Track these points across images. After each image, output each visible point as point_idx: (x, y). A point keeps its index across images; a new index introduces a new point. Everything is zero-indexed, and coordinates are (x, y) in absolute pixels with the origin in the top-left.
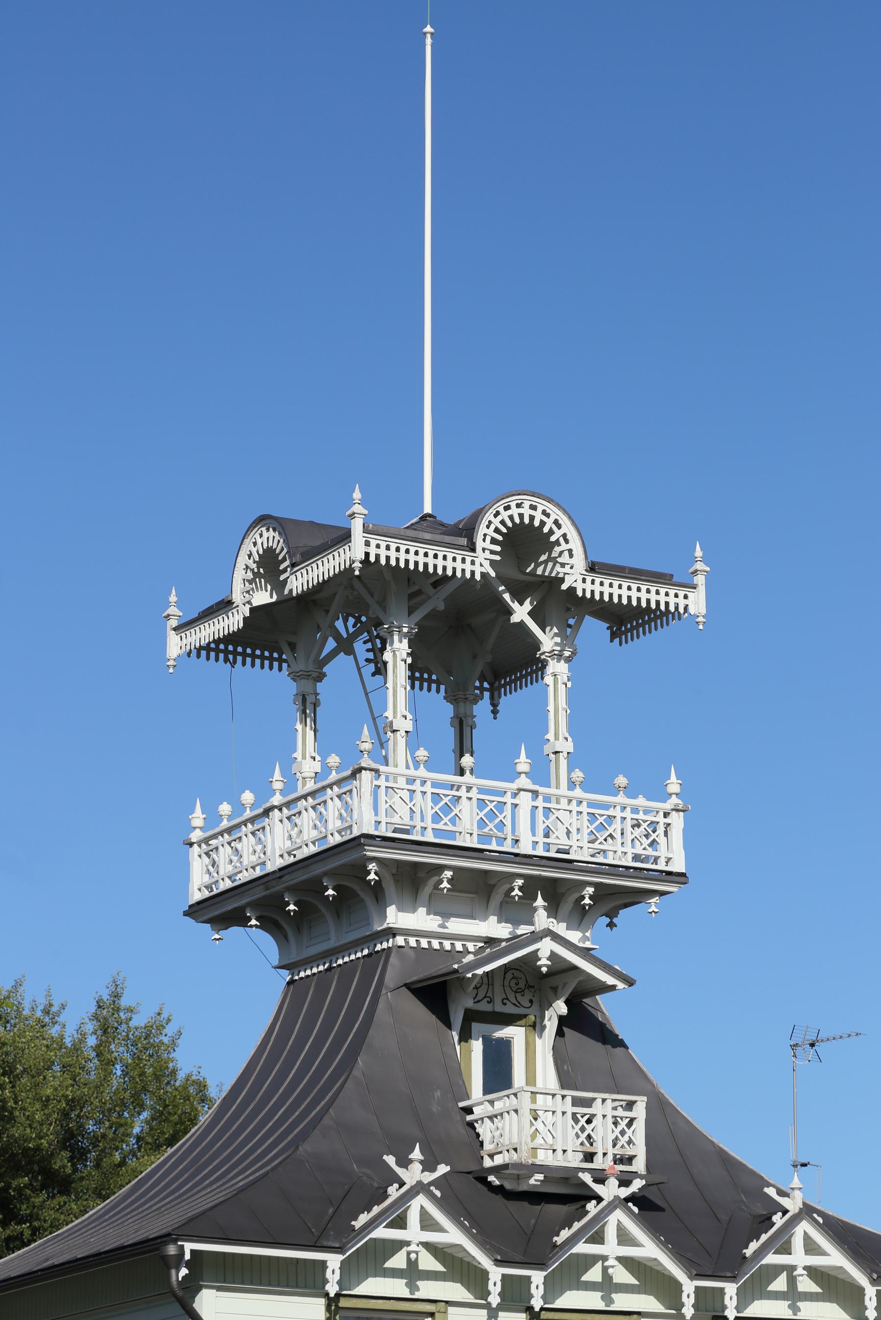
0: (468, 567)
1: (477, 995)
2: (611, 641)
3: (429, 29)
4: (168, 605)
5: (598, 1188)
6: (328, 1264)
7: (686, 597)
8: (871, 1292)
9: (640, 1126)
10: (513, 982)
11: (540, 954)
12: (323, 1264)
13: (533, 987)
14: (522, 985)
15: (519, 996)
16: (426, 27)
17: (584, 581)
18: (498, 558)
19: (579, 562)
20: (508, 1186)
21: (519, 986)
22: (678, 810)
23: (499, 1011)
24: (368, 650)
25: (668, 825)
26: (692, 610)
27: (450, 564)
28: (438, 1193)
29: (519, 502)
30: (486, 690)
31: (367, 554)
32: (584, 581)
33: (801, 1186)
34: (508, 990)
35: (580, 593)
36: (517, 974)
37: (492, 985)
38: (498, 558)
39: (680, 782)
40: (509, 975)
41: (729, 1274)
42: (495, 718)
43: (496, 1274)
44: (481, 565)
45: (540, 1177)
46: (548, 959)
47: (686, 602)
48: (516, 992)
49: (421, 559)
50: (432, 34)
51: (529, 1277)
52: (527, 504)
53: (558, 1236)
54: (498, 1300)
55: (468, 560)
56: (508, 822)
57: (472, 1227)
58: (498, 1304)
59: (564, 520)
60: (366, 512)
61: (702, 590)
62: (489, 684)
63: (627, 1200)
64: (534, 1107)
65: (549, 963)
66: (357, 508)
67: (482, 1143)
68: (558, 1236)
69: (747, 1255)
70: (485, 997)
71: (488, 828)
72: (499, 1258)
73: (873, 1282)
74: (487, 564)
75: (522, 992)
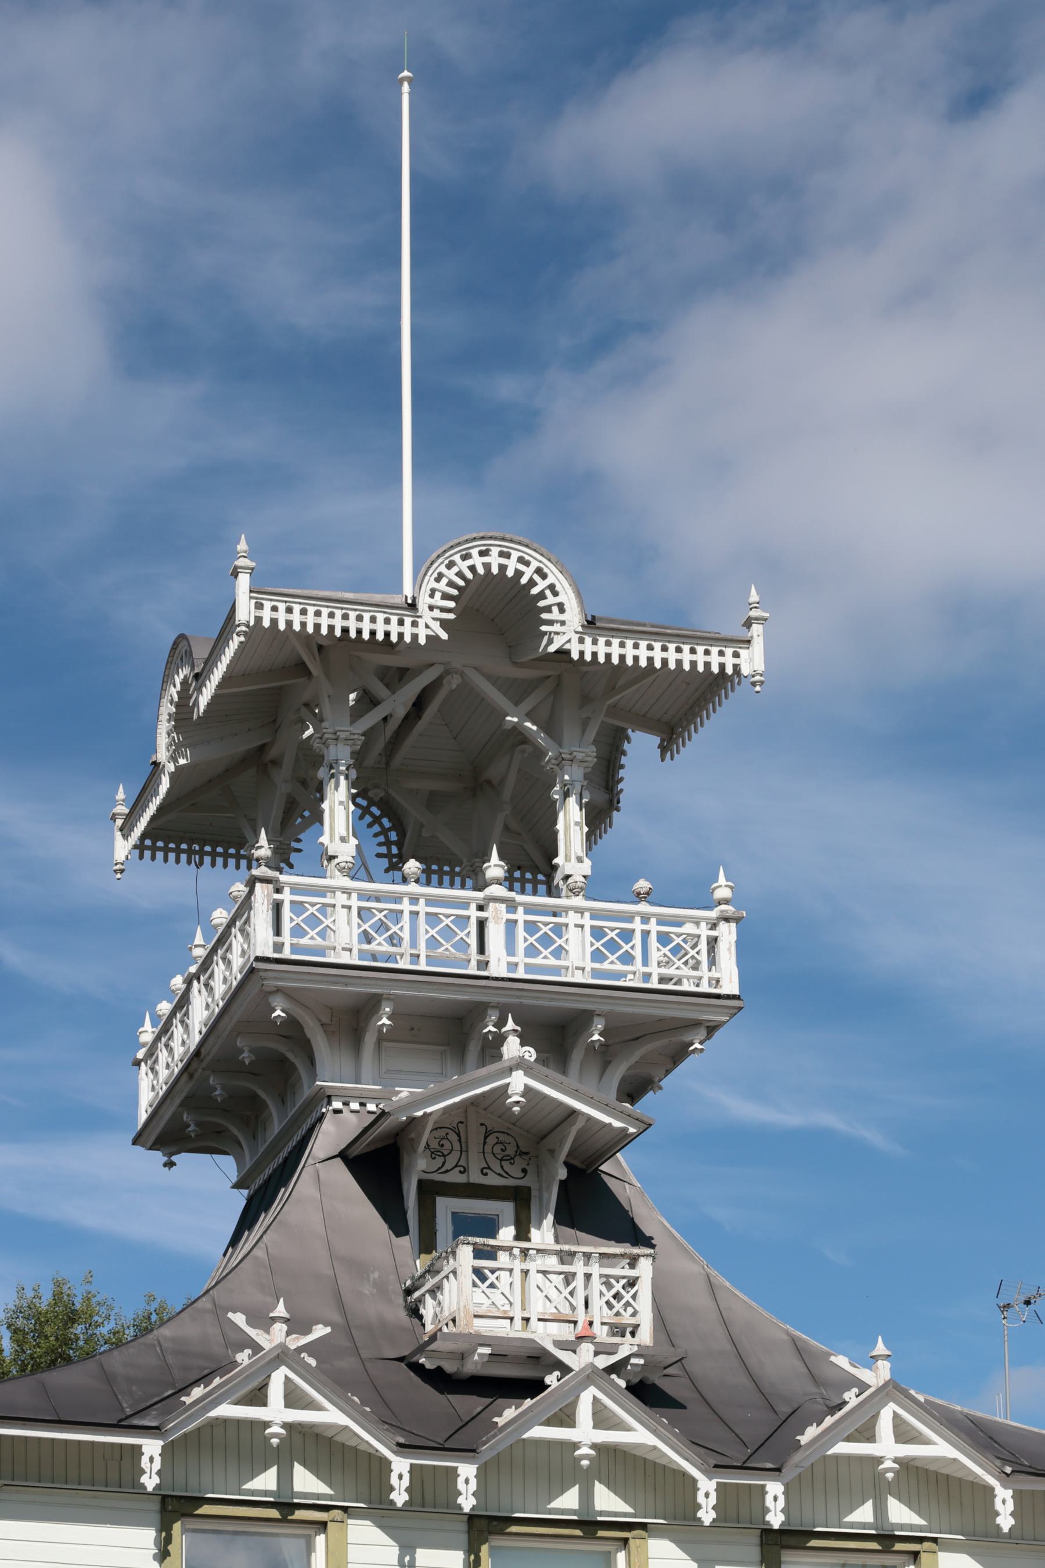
0: (408, 631)
1: (444, 1163)
2: (663, 760)
3: (406, 73)
4: (115, 803)
6: (144, 1450)
9: (645, 1288)
10: (497, 1149)
12: (137, 1451)
13: (527, 1154)
14: (511, 1150)
15: (506, 1164)
17: (581, 641)
19: (574, 617)
20: (450, 1367)
21: (506, 1153)
22: (727, 920)
23: (476, 1182)
24: (380, 844)
25: (716, 939)
26: (745, 671)
28: (312, 1362)
29: (484, 548)
30: (541, 882)
31: (259, 620)
32: (581, 641)
33: (888, 1353)
35: (575, 656)
36: (503, 1138)
37: (467, 1151)
41: (769, 1465)
43: (401, 1466)
44: (427, 626)
45: (487, 1351)
47: (736, 661)
50: (410, 80)
51: (140, 1447)
52: (495, 551)
53: (500, 1415)
54: (405, 1497)
55: (408, 621)
56: (406, 935)
57: (364, 1403)
59: (550, 568)
60: (253, 564)
62: (545, 875)
67: (423, 1325)
68: (500, 1415)
69: (802, 1443)
70: (456, 1166)
71: (443, 948)
72: (402, 1440)
73: (1005, 1478)
74: (436, 627)
75: (511, 1160)
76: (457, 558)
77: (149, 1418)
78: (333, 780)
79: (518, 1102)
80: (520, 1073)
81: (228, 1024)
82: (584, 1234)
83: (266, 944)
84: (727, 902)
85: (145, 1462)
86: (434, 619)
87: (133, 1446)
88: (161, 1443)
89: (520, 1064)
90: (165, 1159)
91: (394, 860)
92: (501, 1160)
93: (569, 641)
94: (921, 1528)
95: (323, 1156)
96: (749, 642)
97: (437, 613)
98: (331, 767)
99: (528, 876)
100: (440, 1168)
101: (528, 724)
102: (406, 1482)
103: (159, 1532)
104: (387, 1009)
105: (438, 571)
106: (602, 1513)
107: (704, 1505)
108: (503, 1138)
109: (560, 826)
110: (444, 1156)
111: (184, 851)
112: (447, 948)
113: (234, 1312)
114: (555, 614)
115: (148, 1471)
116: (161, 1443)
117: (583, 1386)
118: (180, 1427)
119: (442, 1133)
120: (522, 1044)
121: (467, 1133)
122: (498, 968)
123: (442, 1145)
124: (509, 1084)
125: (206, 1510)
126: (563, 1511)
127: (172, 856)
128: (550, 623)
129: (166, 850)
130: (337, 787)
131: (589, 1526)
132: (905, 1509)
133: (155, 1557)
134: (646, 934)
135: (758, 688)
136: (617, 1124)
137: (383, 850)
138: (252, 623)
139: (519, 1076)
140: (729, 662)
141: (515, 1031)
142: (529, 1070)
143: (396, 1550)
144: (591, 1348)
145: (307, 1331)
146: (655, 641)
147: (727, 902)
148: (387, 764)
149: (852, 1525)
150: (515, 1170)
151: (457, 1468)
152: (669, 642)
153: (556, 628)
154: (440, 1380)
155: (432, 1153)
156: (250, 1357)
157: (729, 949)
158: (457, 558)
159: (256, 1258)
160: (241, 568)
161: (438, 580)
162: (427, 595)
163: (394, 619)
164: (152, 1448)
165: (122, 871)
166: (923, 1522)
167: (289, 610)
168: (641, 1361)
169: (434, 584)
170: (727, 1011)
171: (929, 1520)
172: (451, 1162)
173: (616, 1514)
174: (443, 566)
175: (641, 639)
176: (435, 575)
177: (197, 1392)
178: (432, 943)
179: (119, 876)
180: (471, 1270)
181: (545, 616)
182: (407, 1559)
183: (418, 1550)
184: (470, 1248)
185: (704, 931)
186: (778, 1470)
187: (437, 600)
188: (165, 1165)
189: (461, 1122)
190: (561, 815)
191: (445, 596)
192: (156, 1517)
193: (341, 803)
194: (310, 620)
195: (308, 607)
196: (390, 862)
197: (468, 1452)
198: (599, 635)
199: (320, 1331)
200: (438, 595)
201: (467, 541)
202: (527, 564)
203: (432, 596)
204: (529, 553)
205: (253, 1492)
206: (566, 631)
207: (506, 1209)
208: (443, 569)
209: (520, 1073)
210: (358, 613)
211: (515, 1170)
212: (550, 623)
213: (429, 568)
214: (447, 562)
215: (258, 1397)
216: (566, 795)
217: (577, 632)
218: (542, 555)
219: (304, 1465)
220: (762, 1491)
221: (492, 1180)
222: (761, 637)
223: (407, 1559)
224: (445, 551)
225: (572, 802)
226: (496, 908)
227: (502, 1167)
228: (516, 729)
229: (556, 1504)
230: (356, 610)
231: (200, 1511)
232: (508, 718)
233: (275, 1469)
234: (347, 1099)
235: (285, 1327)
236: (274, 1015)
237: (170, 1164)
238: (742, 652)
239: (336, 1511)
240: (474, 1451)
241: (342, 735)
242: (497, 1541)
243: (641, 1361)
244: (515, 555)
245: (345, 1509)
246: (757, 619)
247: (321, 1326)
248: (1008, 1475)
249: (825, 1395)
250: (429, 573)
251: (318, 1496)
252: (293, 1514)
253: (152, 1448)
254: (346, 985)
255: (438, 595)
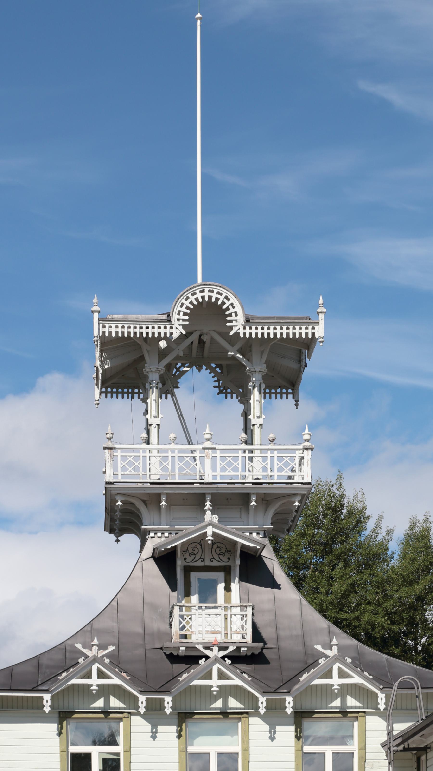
1: (195, 558)
3: (199, 15)
5: (207, 652)
7: (313, 328)
8: (382, 696)
10: (218, 550)
11: (208, 534)
12: (42, 698)
14: (223, 550)
15: (221, 557)
16: (197, 14)
17: (245, 328)
18: (187, 323)
19: (240, 319)
21: (221, 551)
22: (307, 449)
23: (208, 565)
27: (156, 331)
29: (202, 289)
30: (290, 393)
31: (104, 333)
32: (245, 328)
34: (214, 554)
35: (242, 336)
36: (220, 545)
38: (187, 323)
39: (309, 433)
40: (215, 546)
41: (285, 691)
42: (297, 408)
43: (142, 698)
44: (177, 328)
46: (212, 537)
47: (313, 331)
48: (219, 555)
49: (138, 330)
50: (200, 18)
51: (43, 697)
52: (207, 290)
55: (168, 327)
56: (170, 467)
58: (50, 711)
59: (231, 296)
61: (322, 323)
63: (223, 658)
64: (182, 613)
65: (212, 538)
66: (96, 308)
70: (200, 559)
72: (140, 689)
75: (223, 554)
76: (190, 295)
77: (46, 686)
78: (151, 390)
79: (210, 540)
80: (211, 527)
81: (109, 500)
82: (252, 585)
83: (110, 476)
84: (308, 440)
85: (45, 702)
86: (179, 325)
87: (40, 697)
88: (50, 695)
89: (211, 524)
90: (116, 538)
91: (221, 388)
92: (219, 555)
93: (239, 329)
94: (359, 708)
95: (145, 558)
96: (318, 322)
97: (181, 322)
98: (151, 384)
99: (284, 391)
100: (193, 560)
101: (238, 355)
102: (144, 704)
103: (58, 725)
104: (164, 498)
105: (181, 302)
106: (231, 709)
107: (261, 707)
108: (220, 545)
109: (251, 401)
110: (195, 555)
111: (125, 393)
112: (187, 470)
113: (77, 643)
114: (233, 317)
115: (46, 705)
116: (50, 695)
117: (214, 663)
118: (57, 688)
119: (194, 545)
120: (213, 514)
121: (204, 544)
122: (208, 479)
123: (194, 550)
124: (206, 532)
125: (76, 716)
126: (215, 709)
127: (120, 395)
128: (231, 321)
129: (117, 393)
130: (153, 393)
131: (225, 714)
132: (354, 700)
133: (57, 734)
134: (272, 457)
135: (321, 344)
136: (252, 545)
137: (217, 384)
138: (101, 335)
139: (211, 524)
140: (310, 331)
141: (210, 509)
142: (214, 526)
143: (150, 727)
144: (217, 648)
145: (106, 648)
146: (277, 325)
147: (308, 440)
148: (203, 355)
149: (331, 708)
150: (225, 559)
151: (164, 698)
152: (283, 325)
153: (234, 323)
154: (174, 658)
155: (190, 554)
156: (84, 660)
157: (307, 462)
158: (190, 295)
159: (113, 606)
160: (94, 311)
161: (181, 306)
162: (177, 314)
163: (162, 327)
164: (47, 697)
165: (98, 404)
166: (361, 705)
167: (117, 327)
168: (246, 649)
169: (179, 309)
170: (306, 489)
171: (363, 704)
172: (198, 557)
173: (237, 709)
174: (184, 299)
175: (271, 325)
176: (180, 304)
177: (64, 674)
178: (181, 469)
179: (97, 406)
180: (178, 616)
181: (228, 319)
182: (154, 730)
183: (159, 727)
184: (178, 607)
185: (298, 454)
186: (289, 692)
187: (182, 316)
188: (116, 541)
189: (202, 540)
190: (252, 396)
191: (185, 314)
192: (57, 719)
193: (154, 400)
194: (126, 330)
195: (124, 325)
196: (219, 389)
197: (167, 692)
198: (252, 325)
199: (111, 648)
200: (182, 313)
201: (194, 287)
202: (221, 294)
203: (179, 314)
204: (221, 290)
205: (94, 708)
206: (238, 325)
207: (221, 575)
208: (183, 301)
209: (211, 527)
210: (146, 325)
211: (225, 559)
212: (231, 321)
213: (177, 301)
214: (185, 297)
215: (88, 676)
216: (254, 387)
217: (242, 325)
218: (227, 290)
219: (114, 696)
220: (284, 700)
221: (215, 563)
222: (323, 320)
223: (154, 730)
224: (184, 293)
225: (256, 390)
226: (207, 453)
227: (219, 558)
228: (234, 358)
229: (213, 706)
230: (145, 324)
231: (74, 716)
232: (230, 353)
233: (103, 698)
234: (156, 532)
235: (97, 648)
236: (117, 504)
237: (118, 541)
238: (316, 327)
239: (125, 714)
240: (169, 692)
241: (153, 370)
242: (190, 721)
243: (246, 649)
244: (215, 291)
245: (129, 713)
246: (321, 312)
247: (111, 646)
248: (382, 689)
249: (310, 662)
250: (177, 304)
251: (120, 708)
252: (109, 715)
253: (47, 697)
254: (144, 490)
255: (182, 313)
